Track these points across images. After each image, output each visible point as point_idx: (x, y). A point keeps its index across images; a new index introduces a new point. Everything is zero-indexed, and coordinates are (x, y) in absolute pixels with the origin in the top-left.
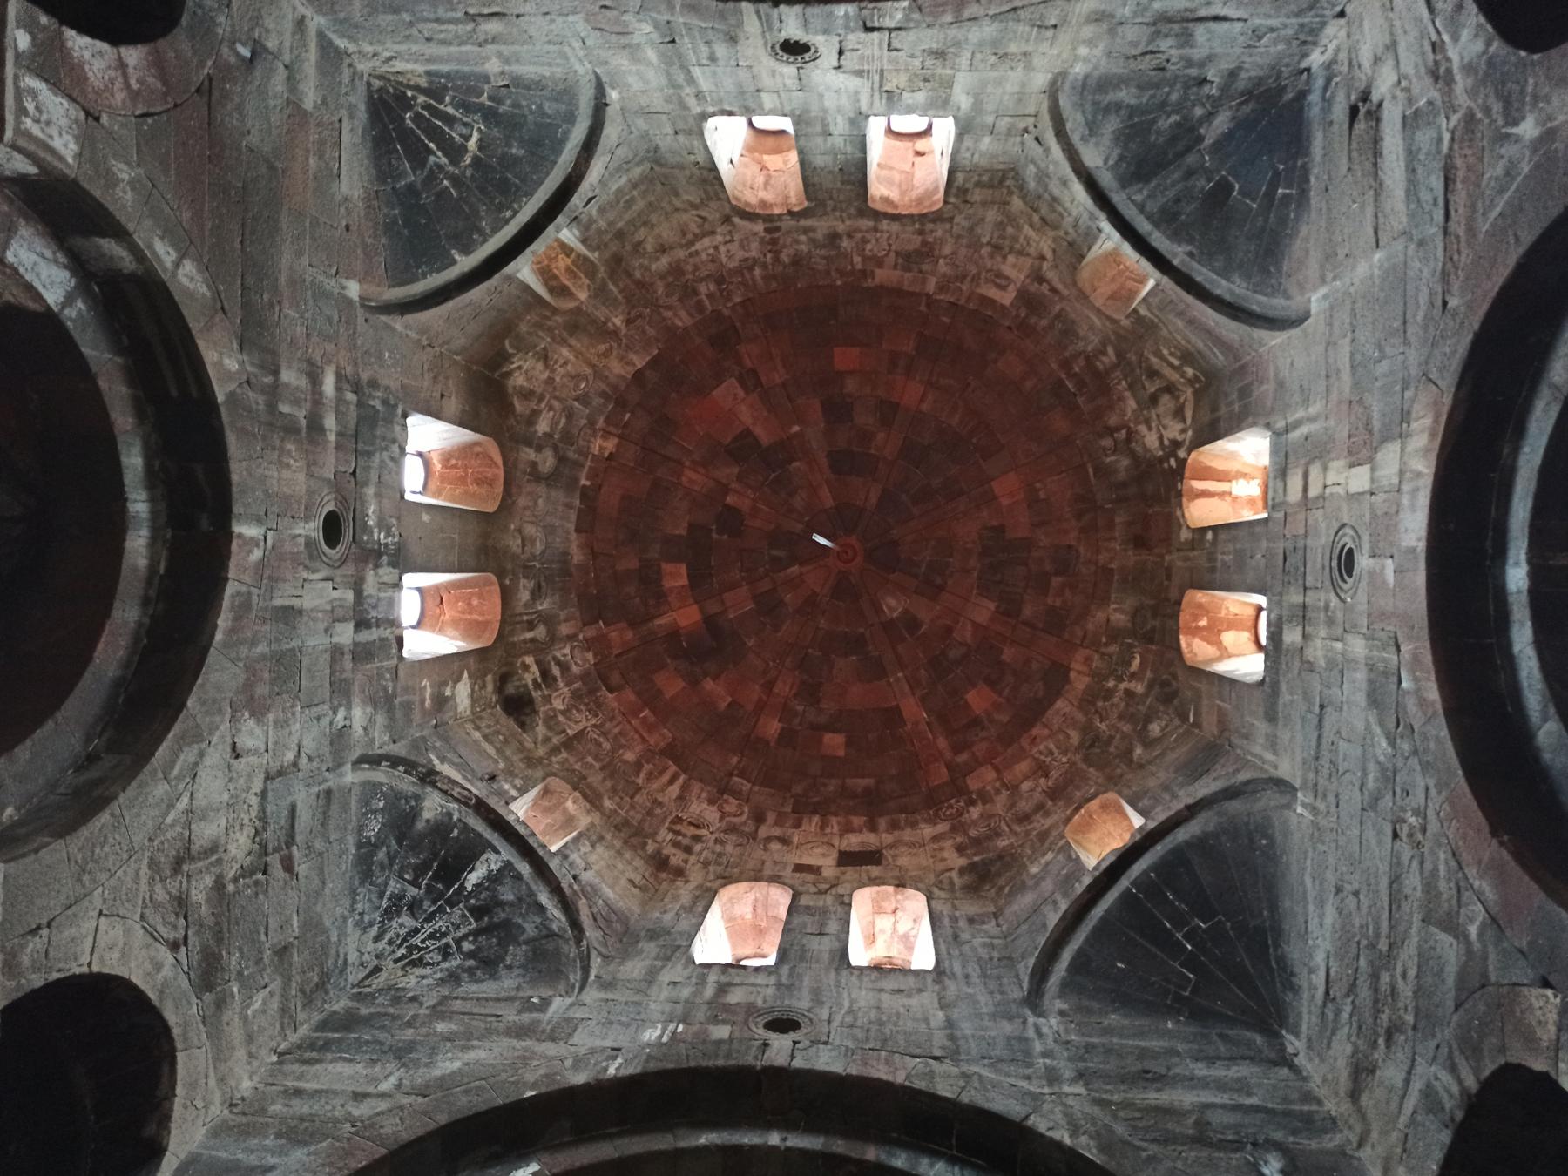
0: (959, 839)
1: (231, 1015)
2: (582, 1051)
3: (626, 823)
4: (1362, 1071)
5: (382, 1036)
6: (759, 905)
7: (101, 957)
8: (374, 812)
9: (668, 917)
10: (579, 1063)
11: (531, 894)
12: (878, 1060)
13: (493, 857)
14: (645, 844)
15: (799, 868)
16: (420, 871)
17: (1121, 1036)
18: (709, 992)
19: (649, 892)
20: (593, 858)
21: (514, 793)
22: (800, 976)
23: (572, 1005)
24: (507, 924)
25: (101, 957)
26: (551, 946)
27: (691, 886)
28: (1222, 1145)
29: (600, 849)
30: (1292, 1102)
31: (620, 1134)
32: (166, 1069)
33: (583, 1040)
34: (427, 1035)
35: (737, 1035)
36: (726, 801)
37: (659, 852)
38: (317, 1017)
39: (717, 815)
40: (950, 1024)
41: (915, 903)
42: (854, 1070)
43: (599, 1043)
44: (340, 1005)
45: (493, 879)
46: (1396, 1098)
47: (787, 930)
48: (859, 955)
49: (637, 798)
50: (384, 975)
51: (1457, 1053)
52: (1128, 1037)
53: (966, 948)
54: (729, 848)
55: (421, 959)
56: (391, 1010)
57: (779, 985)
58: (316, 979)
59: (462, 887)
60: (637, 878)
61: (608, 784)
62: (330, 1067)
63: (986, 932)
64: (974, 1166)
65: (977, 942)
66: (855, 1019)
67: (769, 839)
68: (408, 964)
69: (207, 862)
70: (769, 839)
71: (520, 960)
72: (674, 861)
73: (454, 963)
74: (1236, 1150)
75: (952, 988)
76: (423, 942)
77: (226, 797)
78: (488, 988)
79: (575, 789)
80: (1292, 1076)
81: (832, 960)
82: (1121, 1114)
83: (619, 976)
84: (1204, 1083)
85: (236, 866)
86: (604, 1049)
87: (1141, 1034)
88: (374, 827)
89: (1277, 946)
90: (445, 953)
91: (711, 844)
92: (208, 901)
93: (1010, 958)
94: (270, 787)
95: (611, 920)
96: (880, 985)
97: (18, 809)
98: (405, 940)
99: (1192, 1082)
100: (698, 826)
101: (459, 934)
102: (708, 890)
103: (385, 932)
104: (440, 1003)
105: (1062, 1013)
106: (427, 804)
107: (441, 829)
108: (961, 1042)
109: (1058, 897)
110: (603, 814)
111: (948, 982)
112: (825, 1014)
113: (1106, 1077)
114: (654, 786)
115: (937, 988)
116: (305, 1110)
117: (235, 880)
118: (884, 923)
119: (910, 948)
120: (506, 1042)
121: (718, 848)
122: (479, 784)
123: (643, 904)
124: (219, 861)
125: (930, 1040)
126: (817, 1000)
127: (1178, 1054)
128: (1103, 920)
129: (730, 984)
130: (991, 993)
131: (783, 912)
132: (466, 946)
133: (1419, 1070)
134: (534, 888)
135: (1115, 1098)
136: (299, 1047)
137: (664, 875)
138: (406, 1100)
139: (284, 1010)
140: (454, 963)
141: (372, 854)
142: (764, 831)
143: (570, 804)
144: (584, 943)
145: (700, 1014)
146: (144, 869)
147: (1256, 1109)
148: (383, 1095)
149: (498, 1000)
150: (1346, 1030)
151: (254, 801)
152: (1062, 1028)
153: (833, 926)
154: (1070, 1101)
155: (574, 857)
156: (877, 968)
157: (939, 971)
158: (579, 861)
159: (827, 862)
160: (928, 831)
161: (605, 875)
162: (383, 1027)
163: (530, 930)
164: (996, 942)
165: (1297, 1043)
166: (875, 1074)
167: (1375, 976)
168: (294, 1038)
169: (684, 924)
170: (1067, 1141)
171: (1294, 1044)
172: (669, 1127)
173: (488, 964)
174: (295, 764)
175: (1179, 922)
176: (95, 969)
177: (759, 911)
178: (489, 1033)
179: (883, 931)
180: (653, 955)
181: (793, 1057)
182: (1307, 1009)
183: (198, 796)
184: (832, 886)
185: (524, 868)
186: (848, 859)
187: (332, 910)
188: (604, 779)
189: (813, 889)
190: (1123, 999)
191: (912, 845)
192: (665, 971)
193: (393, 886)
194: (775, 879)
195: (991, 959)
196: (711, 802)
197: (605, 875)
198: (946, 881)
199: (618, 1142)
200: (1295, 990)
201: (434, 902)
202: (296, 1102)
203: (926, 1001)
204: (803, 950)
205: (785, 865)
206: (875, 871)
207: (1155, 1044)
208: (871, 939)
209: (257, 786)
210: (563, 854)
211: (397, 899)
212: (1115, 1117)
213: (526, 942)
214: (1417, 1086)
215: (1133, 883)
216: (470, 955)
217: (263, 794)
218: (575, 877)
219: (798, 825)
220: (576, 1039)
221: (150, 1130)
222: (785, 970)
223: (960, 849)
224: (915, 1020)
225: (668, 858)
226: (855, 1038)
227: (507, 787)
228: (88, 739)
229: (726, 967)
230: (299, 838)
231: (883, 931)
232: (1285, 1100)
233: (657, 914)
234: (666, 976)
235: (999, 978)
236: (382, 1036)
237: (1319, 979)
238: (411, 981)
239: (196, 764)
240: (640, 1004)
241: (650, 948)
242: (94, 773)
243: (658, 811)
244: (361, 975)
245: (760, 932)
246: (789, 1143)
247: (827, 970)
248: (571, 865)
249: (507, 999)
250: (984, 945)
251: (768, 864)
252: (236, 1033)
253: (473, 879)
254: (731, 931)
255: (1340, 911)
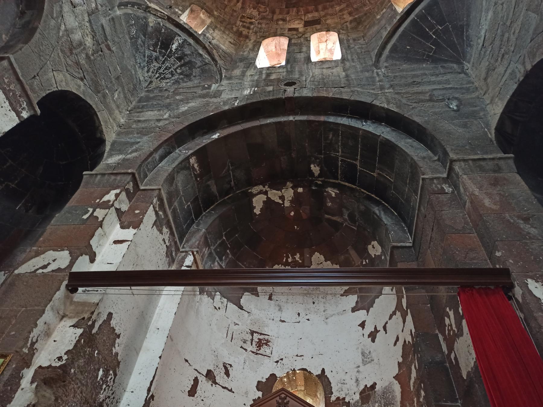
0: (350, 10)
1: (109, 99)
2: (225, 100)
3: (224, 20)
4: (490, 70)
5: (160, 102)
6: (277, 45)
7: (60, 85)
8: (132, 25)
9: (245, 53)
10: (225, 103)
11: (196, 50)
12: (323, 90)
13: (179, 38)
14: (232, 28)
15: (290, 30)
16: (155, 46)
17: (406, 71)
18: (264, 76)
19: (238, 45)
20: (215, 35)
21: (180, 12)
22: (294, 68)
23: (219, 86)
24: (190, 62)
25: (60, 85)
26: (207, 68)
27: (252, 41)
28: (438, 101)
29: (216, 31)
30: (464, 85)
31: (242, 123)
32: (95, 117)
33: (225, 96)
34: (174, 100)
35: (275, 89)
36: (260, 7)
37: (238, 30)
38: (137, 99)
39: (257, 13)
40: (347, 76)
41: (334, 37)
42: (315, 95)
43: (230, 97)
44: (143, 94)
45: (181, 46)
46: (500, 77)
47: (288, 52)
48: (314, 58)
49: (226, 10)
50: (154, 83)
51: (526, 57)
52: (408, 72)
53: (352, 50)
54: (263, 26)
55: (164, 77)
56: (160, 94)
57: (287, 71)
58: (132, 87)
59: (171, 50)
60: (232, 41)
61: (214, 5)
62: (146, 113)
63: (360, 43)
64: (355, 118)
65: (356, 47)
66: (315, 79)
67: (278, 20)
68: (161, 79)
69: (80, 49)
70: (278, 20)
71: (198, 74)
72: (244, 33)
73: (176, 77)
74: (442, 102)
75: (348, 64)
76: (163, 71)
77: (77, 24)
78: (190, 84)
79: (202, 9)
80: (465, 76)
81: (305, 60)
82: (405, 96)
83: (233, 75)
84: (434, 83)
85: (91, 50)
86: (232, 98)
87: (413, 70)
88: (134, 31)
89: (467, 31)
90: (173, 75)
91: (257, 25)
92: (86, 63)
93: (369, 51)
94: (91, 18)
95: (225, 56)
96: (322, 67)
97: (6, 35)
98: (157, 71)
99: (430, 83)
100: (251, 19)
101: (175, 67)
102: (258, 42)
103: (150, 69)
104: (175, 90)
105: (386, 67)
106: (150, 20)
107: (157, 29)
108: (351, 81)
109: (387, 26)
110: (215, 18)
111: (346, 62)
112: (304, 78)
113: (401, 86)
114: (232, 4)
115: (342, 65)
116: (143, 126)
117: (93, 55)
118: (323, 46)
119: (332, 54)
120: (200, 100)
121: (259, 26)
122: (166, 10)
123: (236, 50)
124: (84, 49)
125: (340, 82)
126: (301, 74)
127: (426, 74)
128: (404, 32)
129: (271, 73)
130: (361, 64)
131: (286, 47)
132: (179, 71)
133: (511, 66)
134: (196, 48)
135: (403, 91)
136: (134, 108)
137: (241, 39)
138: (173, 120)
139: (125, 97)
140: (176, 77)
141: (136, 42)
142: (275, 17)
143: (202, 15)
144: (218, 65)
145: (262, 84)
146: (60, 54)
147: (451, 88)
148: (166, 119)
149: (194, 87)
150: (487, 57)
151: (88, 24)
152: (386, 72)
153: (304, 49)
154: (387, 94)
155: (208, 35)
156: (322, 62)
157: (343, 59)
158: (210, 36)
159: (299, 25)
160: (338, 8)
161: (220, 40)
162: (159, 100)
163: (199, 64)
164: (363, 46)
165: (469, 65)
166: (322, 95)
167: (503, 35)
168: (132, 106)
169: (252, 55)
170: (386, 106)
171: (467, 65)
172: (258, 119)
173: (188, 76)
174: (97, 8)
175: (431, 27)
176: (60, 89)
177: (277, 47)
178: (193, 98)
179: (322, 49)
180: (243, 67)
181: (294, 93)
182: (473, 53)
183: (67, 24)
184: (303, 35)
185: (191, 41)
186: (307, 24)
187: (130, 63)
188: (213, 3)
189: (296, 37)
190: (408, 59)
191: (332, 15)
192: (248, 71)
193: (147, 53)
194: (282, 35)
195: (362, 52)
196: (254, 8)
197: (220, 40)
198: (345, 27)
199: (242, 125)
200: (471, 46)
201: (163, 57)
202: (140, 124)
203: (339, 70)
204: (295, 58)
205: (284, 29)
206: (318, 27)
207: (419, 72)
208: (318, 52)
209: (87, 19)
210: (203, 34)
211: (150, 57)
212: (402, 97)
213: (199, 67)
214: (509, 71)
215: (416, 16)
216: (181, 74)
217: (90, 21)
218: (210, 42)
219: (288, 13)
220: (223, 96)
221: (99, 135)
222: (289, 66)
223: (350, 14)
224: (334, 76)
225: (242, 32)
226: (315, 85)
227: (177, 10)
228: (18, 6)
229: (268, 68)
230: (109, 38)
231: (322, 49)
232: (461, 84)
233: (242, 53)
234: (249, 73)
235: (364, 58)
236: (160, 102)
237: (481, 41)
238: (163, 84)
239: (61, 11)
240: (241, 83)
241: (241, 65)
242: (27, 18)
243: (235, 14)
244: (146, 85)
245: (278, 55)
246: (296, 119)
247: (303, 64)
248: (207, 38)
249: (197, 87)
250: (359, 48)
251: (279, 30)
252: (114, 106)
253: (174, 47)
254: (270, 54)
255: (494, 12)
